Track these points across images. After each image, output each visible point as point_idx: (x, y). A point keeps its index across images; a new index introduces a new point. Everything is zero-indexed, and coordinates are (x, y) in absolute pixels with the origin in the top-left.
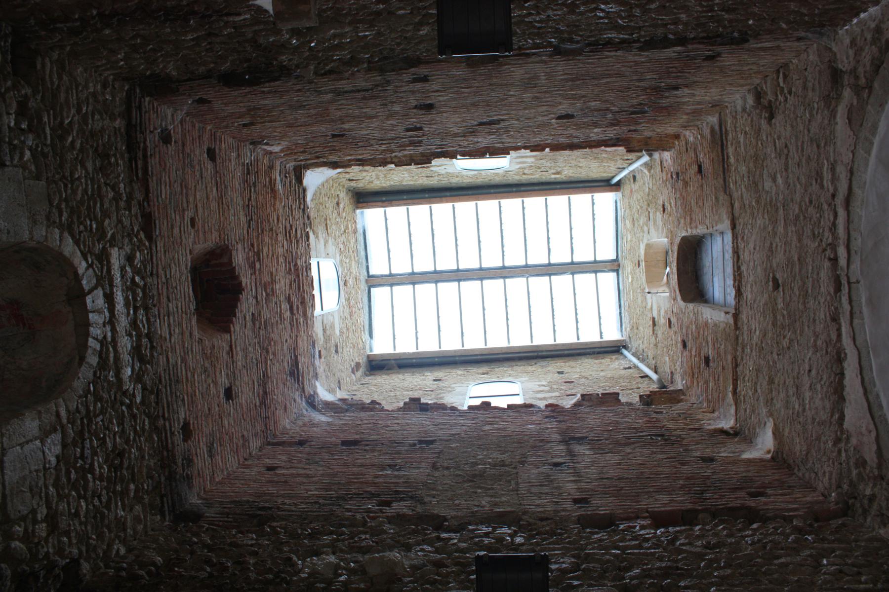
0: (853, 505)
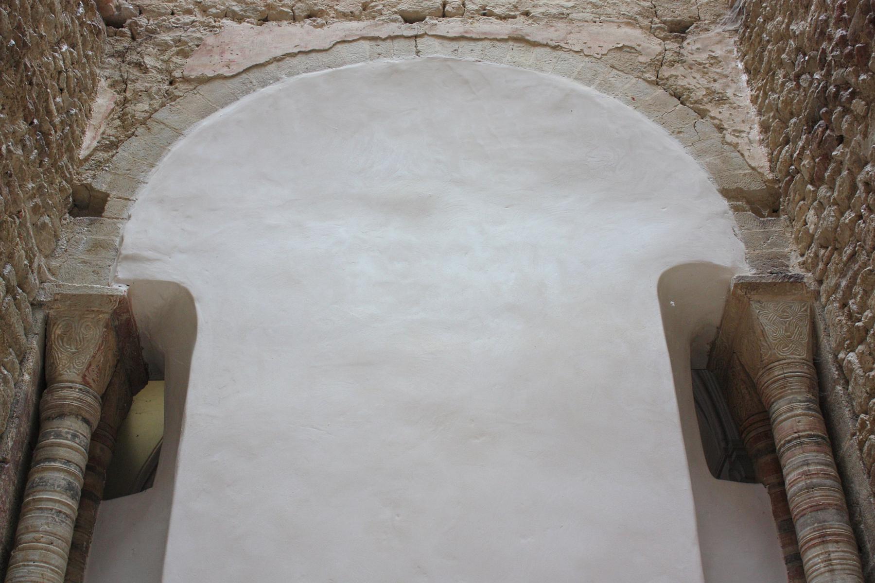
0: (123, 35)
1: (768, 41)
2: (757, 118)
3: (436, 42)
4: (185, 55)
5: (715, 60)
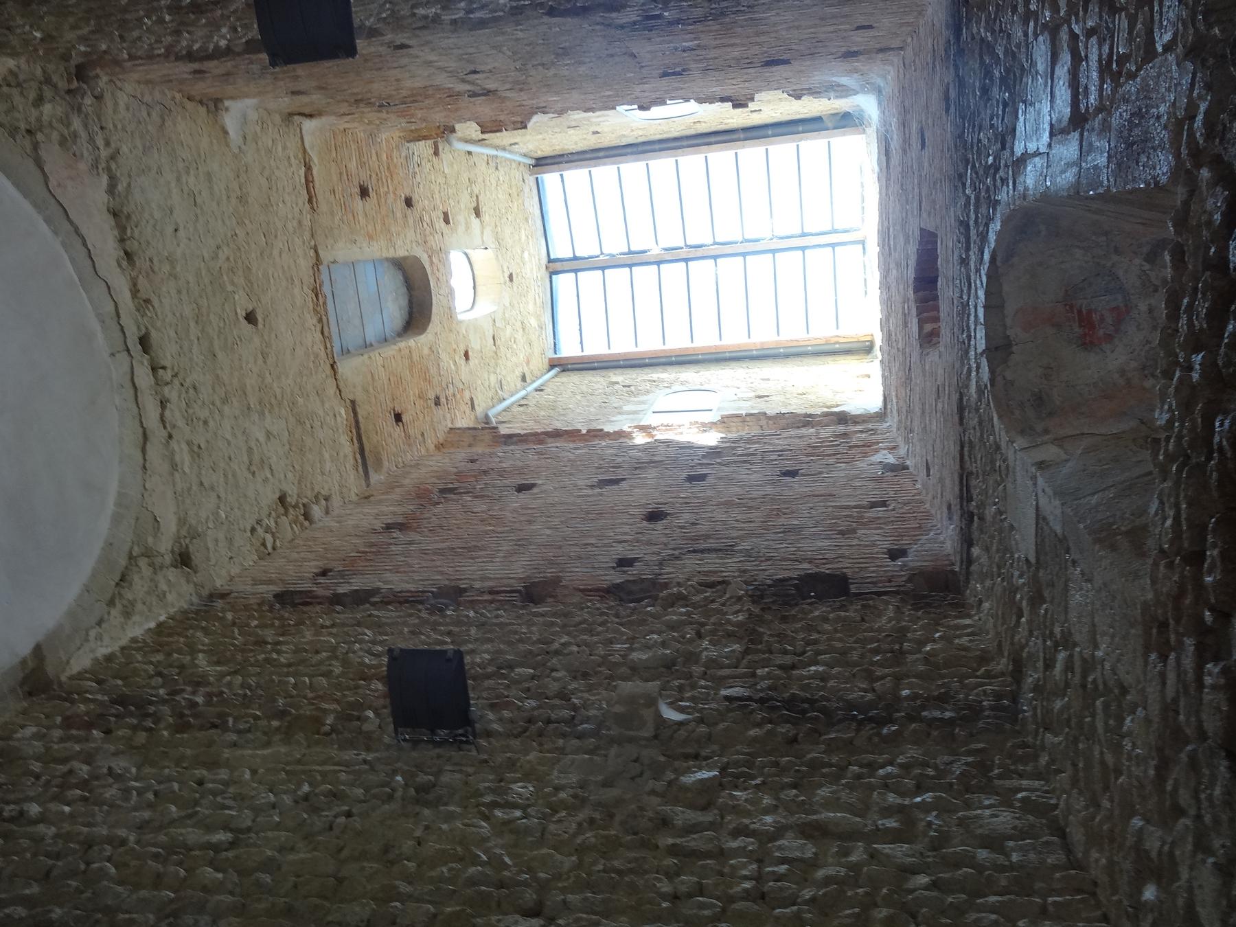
0: (69, 81)
1: (187, 637)
2: (117, 648)
3: (126, 368)
4: (63, 142)
5: (162, 597)
